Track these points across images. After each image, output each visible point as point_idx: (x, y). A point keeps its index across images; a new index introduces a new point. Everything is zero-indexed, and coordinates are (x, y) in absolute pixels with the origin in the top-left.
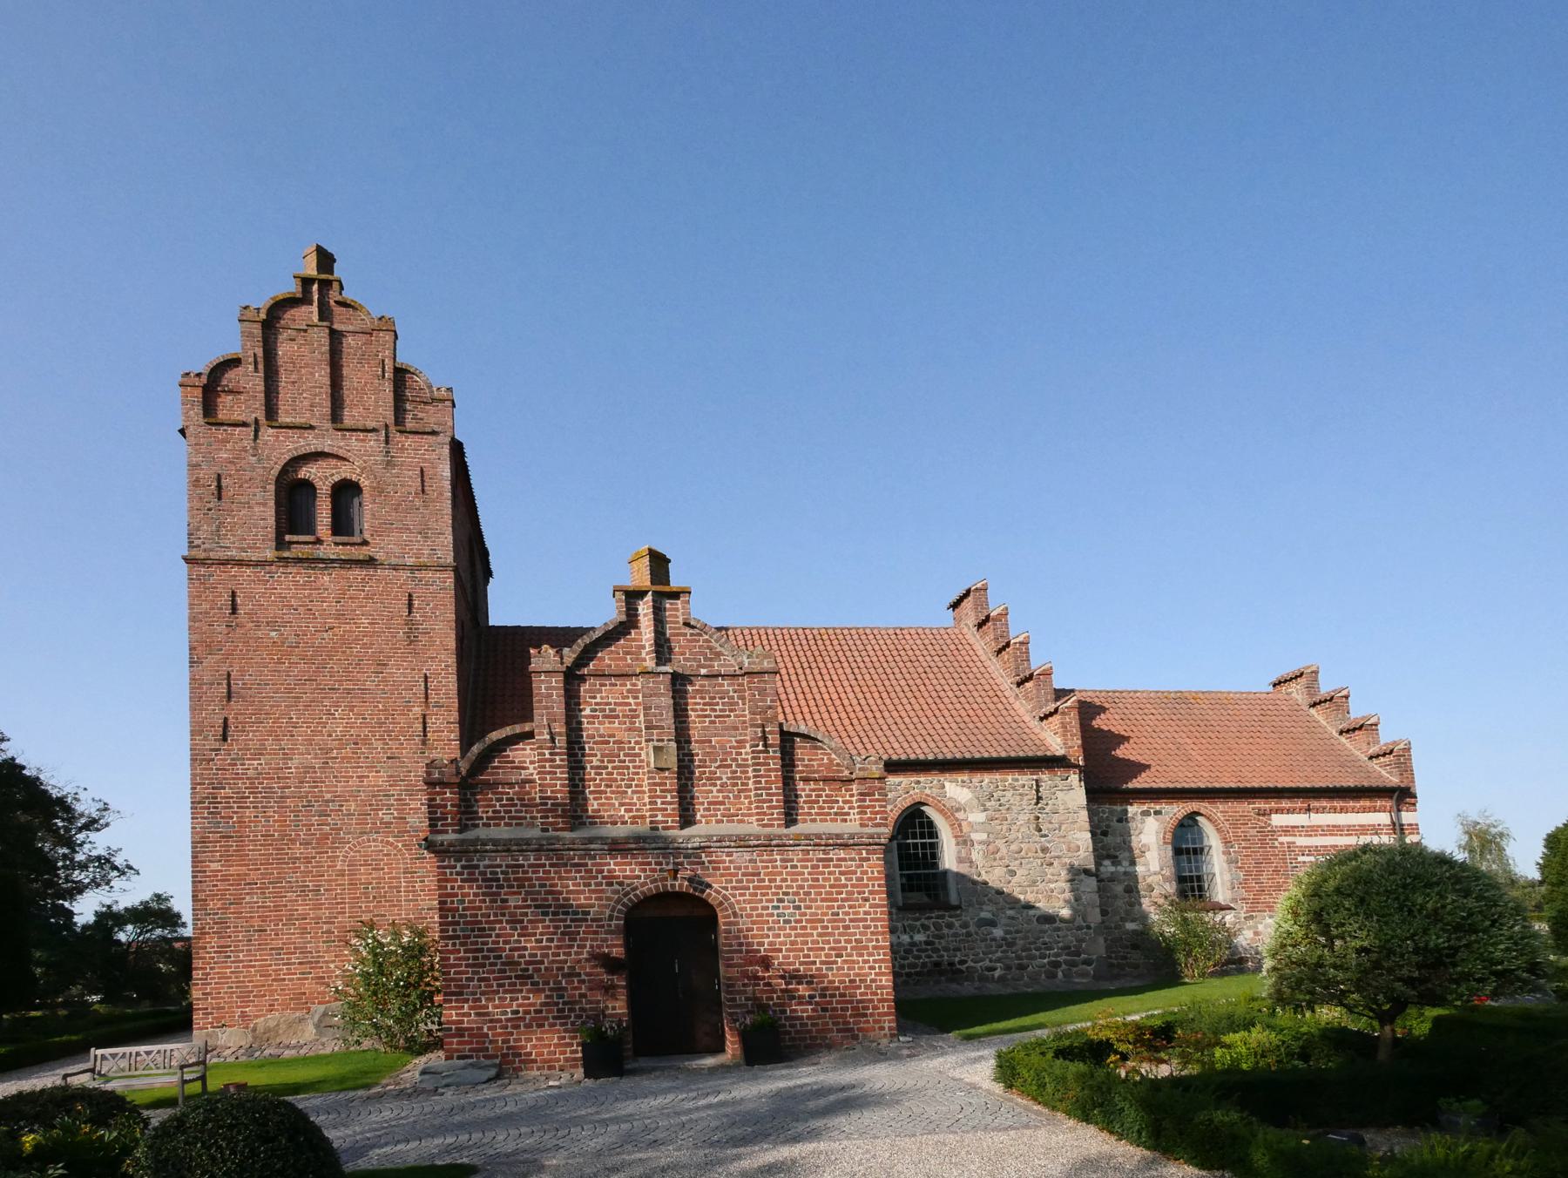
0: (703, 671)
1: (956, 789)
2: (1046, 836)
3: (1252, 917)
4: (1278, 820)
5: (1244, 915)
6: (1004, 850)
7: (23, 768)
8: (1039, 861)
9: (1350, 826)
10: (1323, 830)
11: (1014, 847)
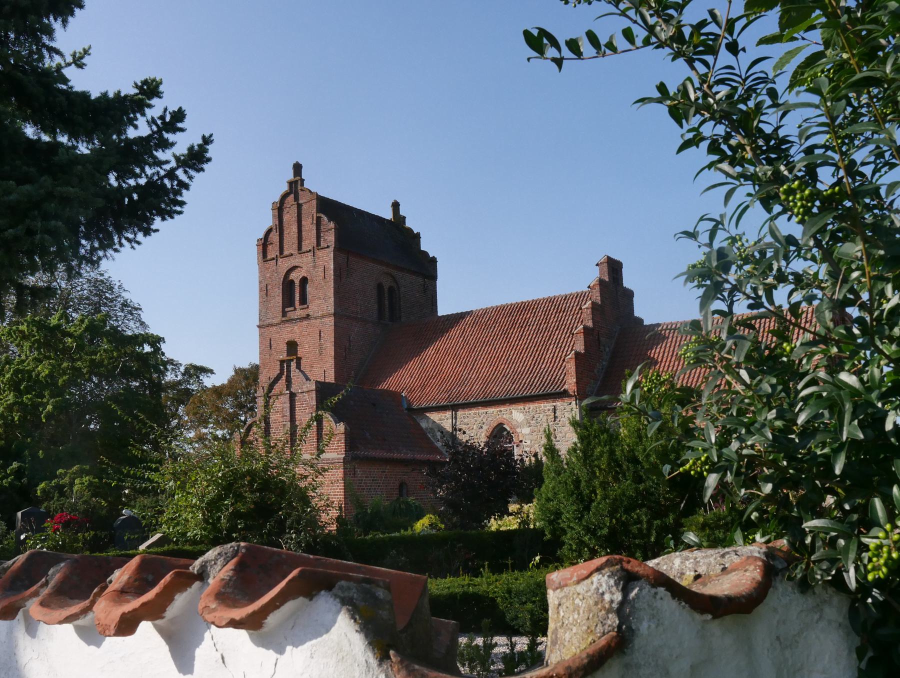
7: (105, 95)
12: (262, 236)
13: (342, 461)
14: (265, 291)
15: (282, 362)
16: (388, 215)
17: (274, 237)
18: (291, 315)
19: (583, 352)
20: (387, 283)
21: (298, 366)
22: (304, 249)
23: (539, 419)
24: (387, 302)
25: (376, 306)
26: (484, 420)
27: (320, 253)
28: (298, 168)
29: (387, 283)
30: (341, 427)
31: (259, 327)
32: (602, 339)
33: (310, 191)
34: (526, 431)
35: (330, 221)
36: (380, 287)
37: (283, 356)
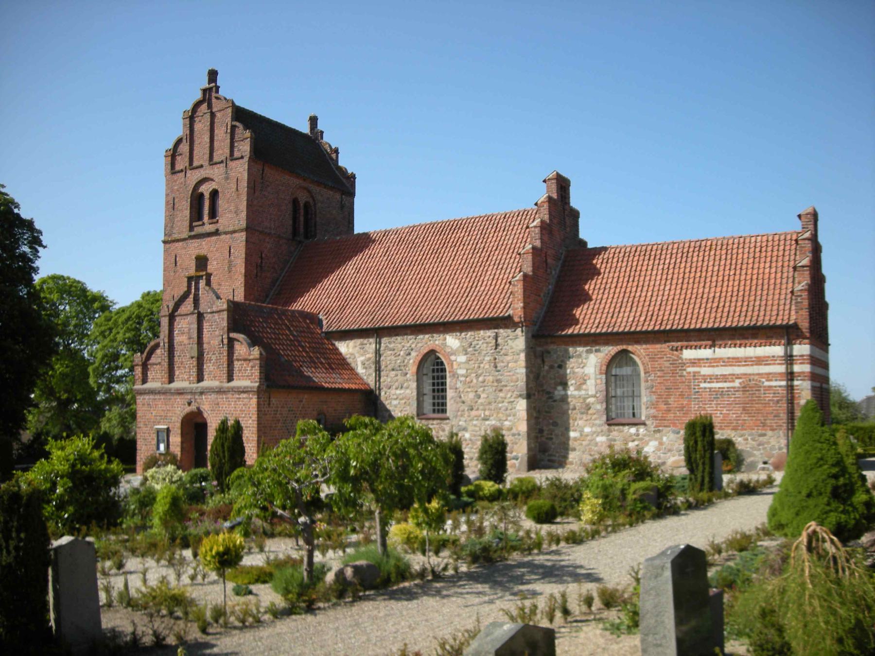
0: (209, 311)
1: (452, 341)
2: (499, 371)
3: (659, 431)
4: (688, 354)
5: (653, 429)
6: (475, 381)
8: (494, 388)
9: (747, 358)
10: (723, 362)
11: (481, 379)
12: (171, 146)
13: (255, 390)
14: (172, 205)
15: (190, 279)
16: (305, 129)
17: (184, 148)
18: (198, 230)
19: (531, 273)
20: (303, 198)
21: (208, 283)
22: (216, 159)
23: (478, 346)
24: (302, 219)
25: (291, 222)
26: (413, 346)
27: (232, 164)
28: (213, 75)
29: (303, 198)
30: (256, 352)
31: (165, 242)
32: (549, 261)
33: (225, 99)
34: (462, 358)
35: (245, 129)
36: (295, 202)
37: (192, 272)
